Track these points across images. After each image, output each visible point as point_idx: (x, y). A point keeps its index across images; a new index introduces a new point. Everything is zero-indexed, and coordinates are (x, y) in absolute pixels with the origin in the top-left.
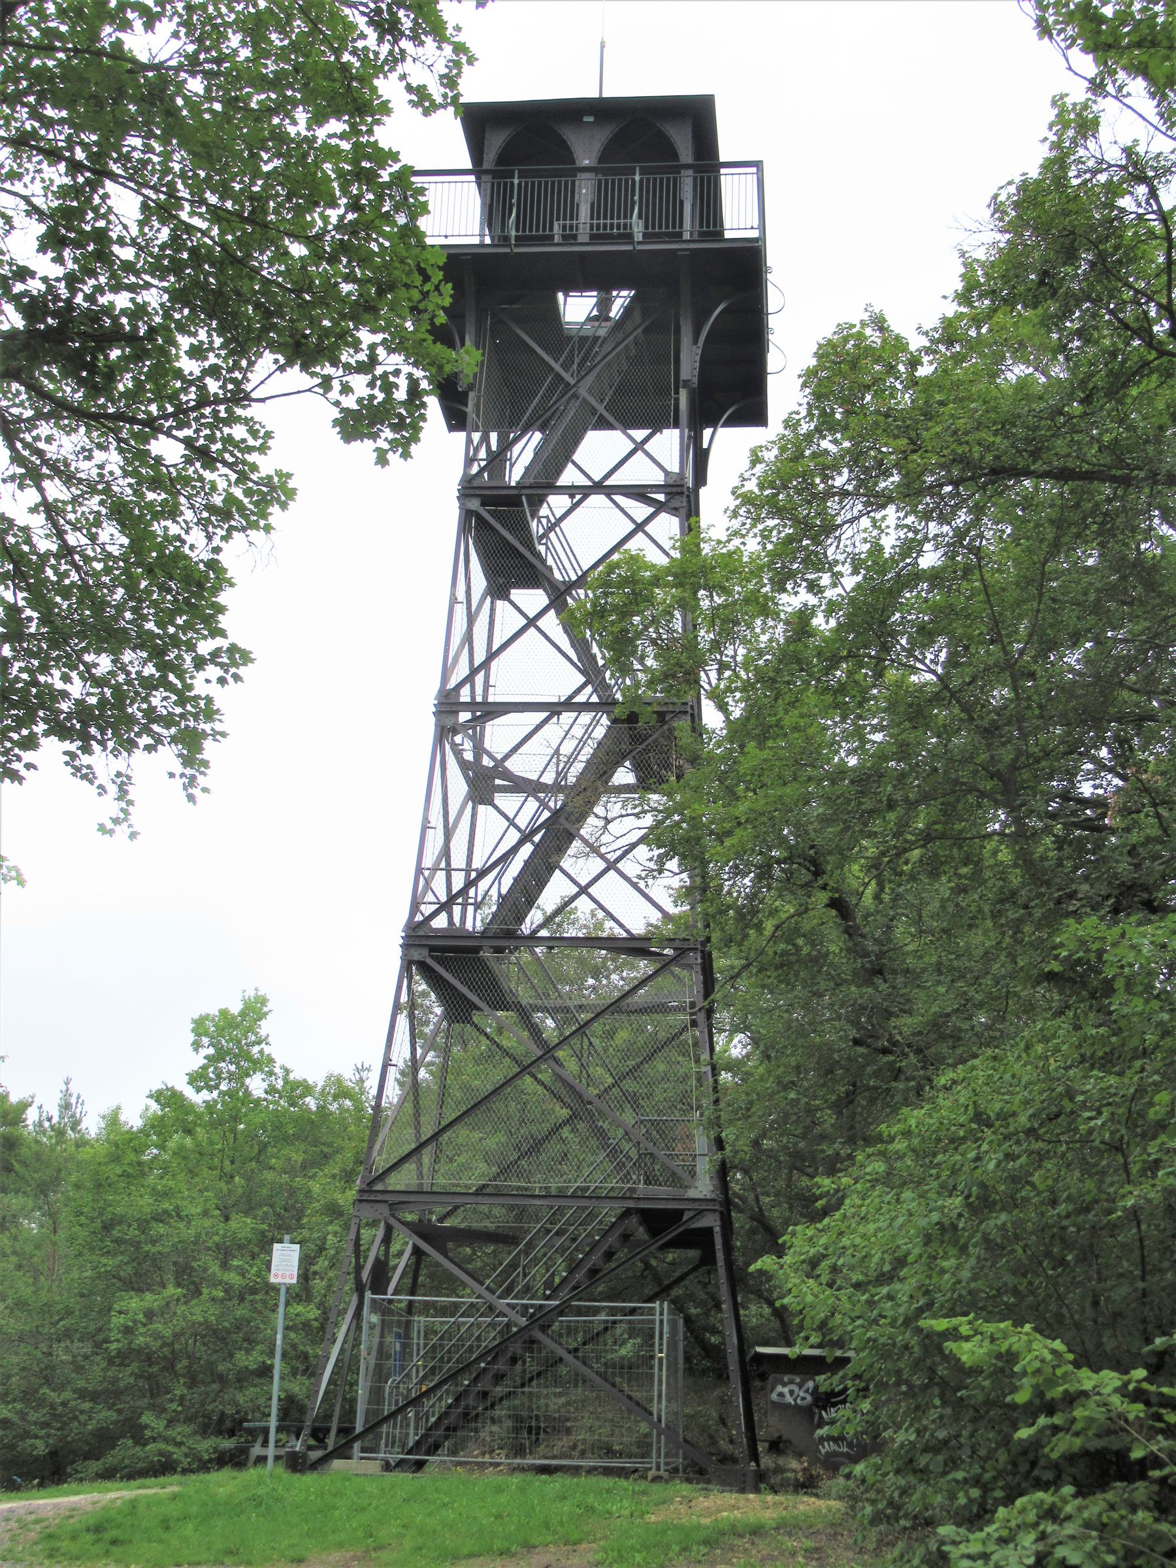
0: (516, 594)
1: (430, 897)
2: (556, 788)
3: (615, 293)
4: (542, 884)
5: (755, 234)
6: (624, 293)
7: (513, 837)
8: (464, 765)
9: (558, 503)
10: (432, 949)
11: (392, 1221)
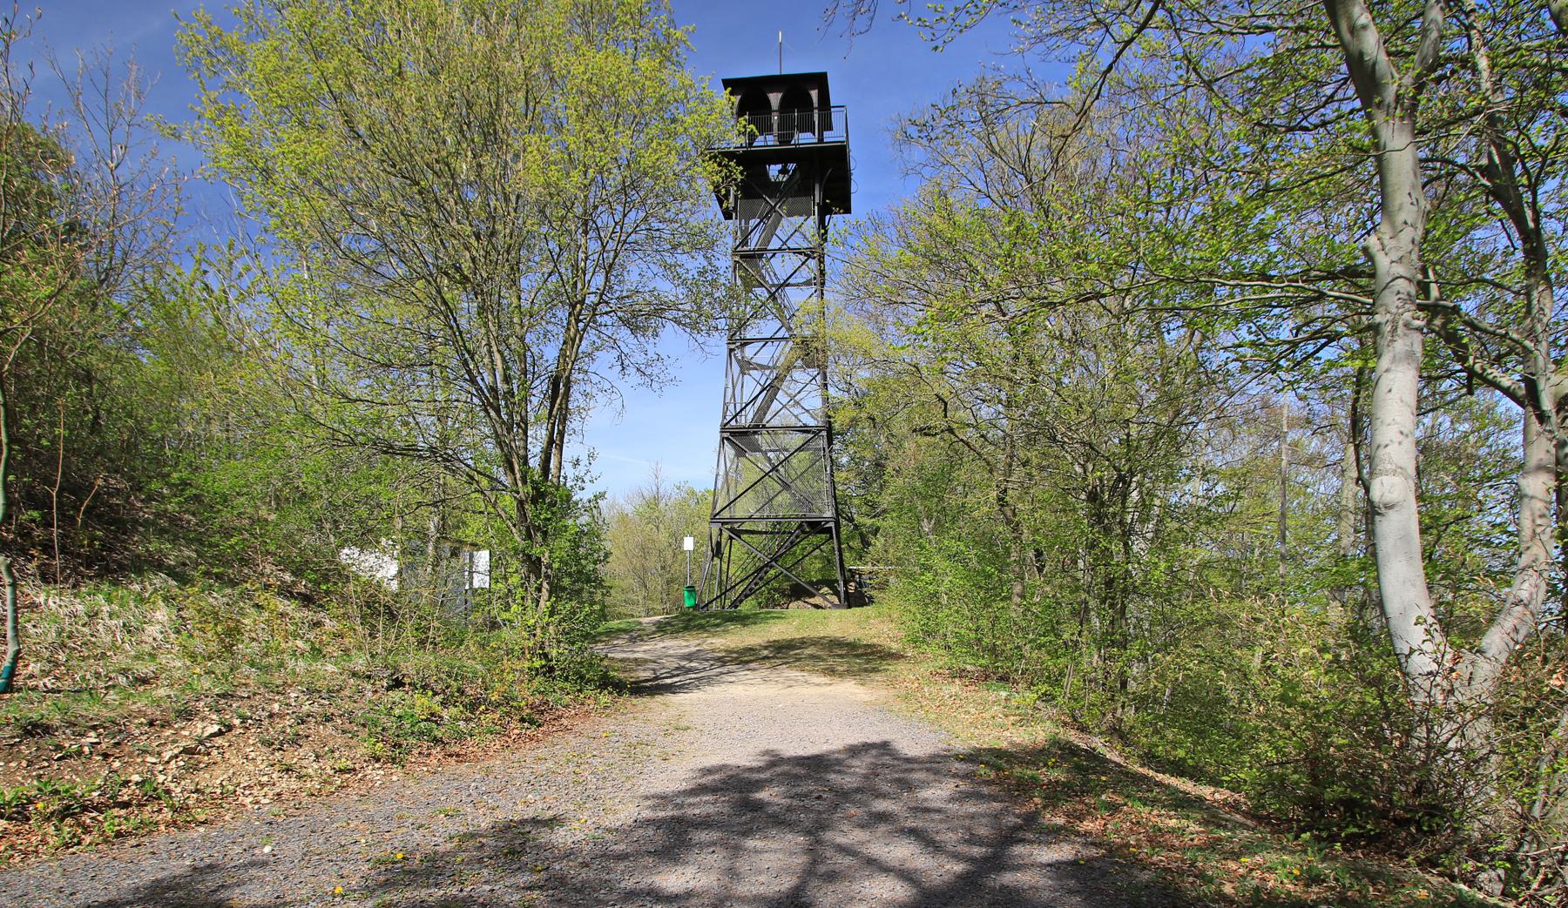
7: (759, 388)
8: (738, 361)
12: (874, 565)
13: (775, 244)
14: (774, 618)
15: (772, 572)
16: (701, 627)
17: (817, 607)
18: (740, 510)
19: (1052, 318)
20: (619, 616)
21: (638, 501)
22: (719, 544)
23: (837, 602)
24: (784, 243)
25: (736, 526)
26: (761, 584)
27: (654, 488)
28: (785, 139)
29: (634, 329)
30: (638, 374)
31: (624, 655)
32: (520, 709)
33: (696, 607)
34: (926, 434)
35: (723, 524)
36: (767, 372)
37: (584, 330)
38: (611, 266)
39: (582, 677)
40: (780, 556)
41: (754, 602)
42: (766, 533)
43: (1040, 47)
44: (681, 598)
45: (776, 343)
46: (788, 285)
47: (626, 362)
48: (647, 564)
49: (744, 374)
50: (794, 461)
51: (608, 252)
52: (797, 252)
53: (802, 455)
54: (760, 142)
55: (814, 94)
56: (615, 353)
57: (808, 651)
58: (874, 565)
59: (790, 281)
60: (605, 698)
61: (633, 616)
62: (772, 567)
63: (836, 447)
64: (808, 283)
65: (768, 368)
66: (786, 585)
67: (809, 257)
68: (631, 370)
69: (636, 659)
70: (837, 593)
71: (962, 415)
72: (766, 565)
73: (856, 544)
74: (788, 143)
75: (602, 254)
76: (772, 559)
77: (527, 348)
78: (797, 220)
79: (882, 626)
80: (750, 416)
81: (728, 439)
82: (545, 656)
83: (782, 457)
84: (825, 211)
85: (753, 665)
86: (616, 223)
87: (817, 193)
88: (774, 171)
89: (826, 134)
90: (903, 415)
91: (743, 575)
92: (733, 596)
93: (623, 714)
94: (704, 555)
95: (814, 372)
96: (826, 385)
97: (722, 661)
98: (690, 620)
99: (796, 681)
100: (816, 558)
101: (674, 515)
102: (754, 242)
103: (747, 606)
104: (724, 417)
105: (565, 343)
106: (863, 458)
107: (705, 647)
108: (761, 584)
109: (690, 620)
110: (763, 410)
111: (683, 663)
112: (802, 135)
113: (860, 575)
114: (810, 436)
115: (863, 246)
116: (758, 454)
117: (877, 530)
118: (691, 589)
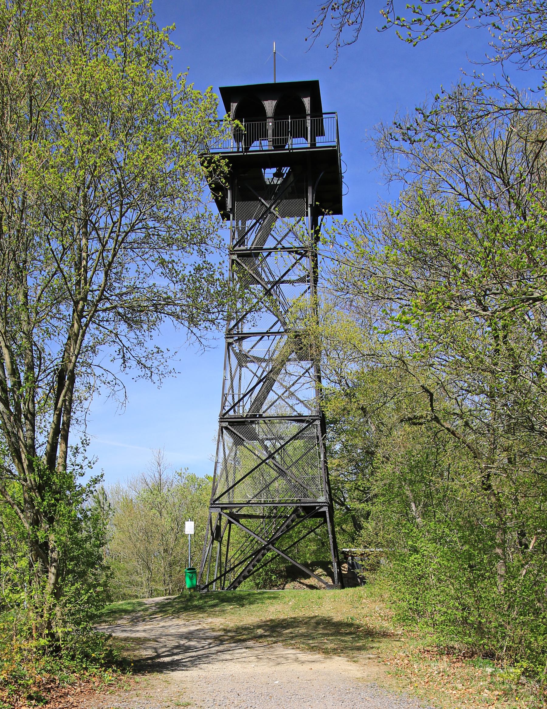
1: (227, 404)
2: (271, 359)
4: (265, 398)
5: (335, 144)
7: (256, 380)
8: (236, 354)
10: (229, 422)
11: (222, 513)
12: (365, 547)
13: (270, 243)
14: (269, 598)
15: (269, 554)
16: (200, 609)
17: (312, 587)
18: (238, 497)
19: (530, 313)
20: (124, 597)
21: (141, 487)
22: (218, 528)
23: (330, 582)
24: (279, 243)
25: (234, 510)
26: (258, 565)
27: (157, 475)
28: (279, 145)
29: (131, 323)
30: (139, 367)
32: (27, 687)
33: (195, 588)
34: (415, 424)
35: (222, 508)
36: (264, 365)
37: (87, 325)
38: (110, 264)
39: (87, 656)
41: (252, 583)
42: (263, 517)
43: (517, 57)
44: (181, 581)
45: (272, 337)
46: (283, 282)
47: (128, 355)
49: (240, 366)
50: (289, 449)
51: (108, 251)
52: (290, 251)
53: (298, 443)
54: (255, 146)
55: (307, 101)
56: (117, 347)
57: (303, 630)
58: (365, 547)
59: (285, 278)
60: (108, 676)
61: (137, 597)
62: (269, 550)
63: (330, 434)
64: (302, 280)
65: (264, 360)
66: (282, 567)
67: (302, 255)
68: (132, 363)
70: (330, 574)
71: (448, 404)
72: (264, 548)
73: (349, 527)
74: (283, 148)
75: (102, 252)
76: (269, 543)
77: (32, 343)
78: (291, 221)
79: (373, 605)
81: (226, 428)
82: (52, 635)
83: (278, 445)
84: (316, 213)
85: (250, 643)
86: (114, 223)
88: (269, 174)
89: (318, 139)
90: (391, 405)
91: (242, 558)
92: (232, 577)
93: (126, 691)
94: (205, 538)
95: (306, 364)
96: (319, 378)
97: (220, 640)
99: (287, 659)
100: (310, 541)
101: (176, 500)
102: (250, 242)
103: (244, 588)
104: (223, 408)
105: (69, 339)
106: (355, 446)
108: (258, 565)
110: (259, 401)
111: (182, 642)
112: (295, 140)
113: (353, 557)
114: (305, 425)
115: (351, 245)
116: (256, 443)
117: (368, 513)
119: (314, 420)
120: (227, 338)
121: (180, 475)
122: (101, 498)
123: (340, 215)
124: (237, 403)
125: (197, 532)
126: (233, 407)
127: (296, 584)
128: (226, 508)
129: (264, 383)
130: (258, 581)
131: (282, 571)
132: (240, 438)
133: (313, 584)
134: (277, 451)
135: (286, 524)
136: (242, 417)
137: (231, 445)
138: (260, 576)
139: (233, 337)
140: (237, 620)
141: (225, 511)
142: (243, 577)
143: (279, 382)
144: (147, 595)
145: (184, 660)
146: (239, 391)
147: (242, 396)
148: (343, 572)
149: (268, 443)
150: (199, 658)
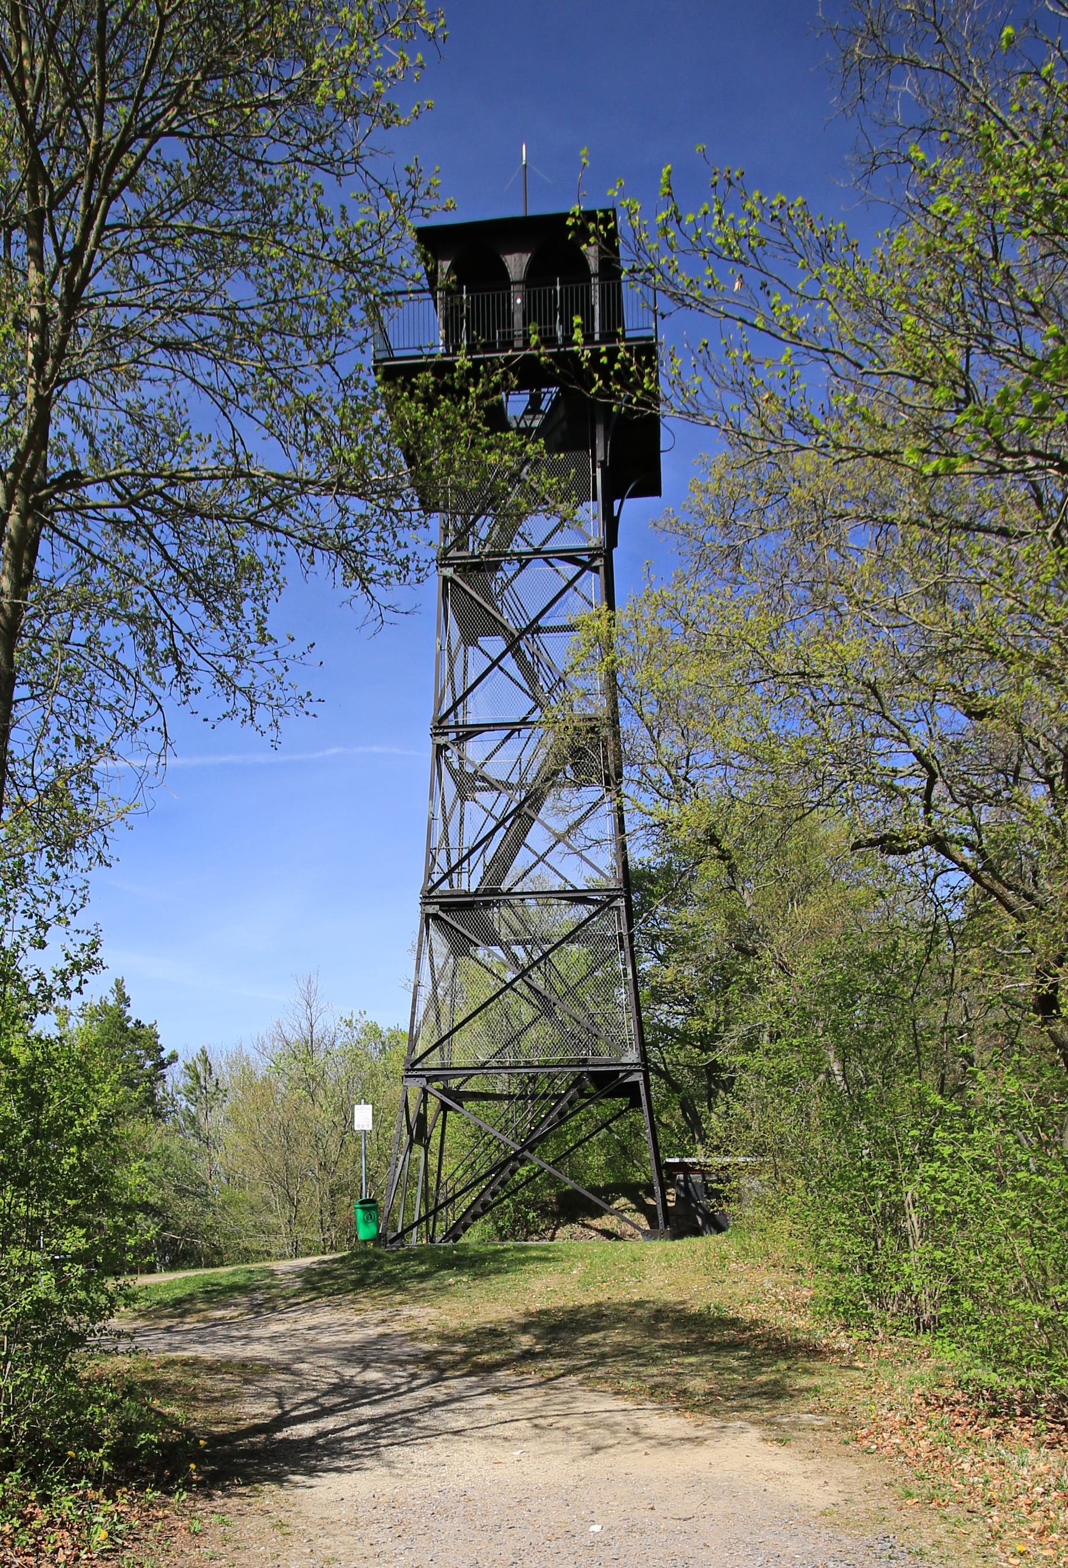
0: (482, 641)
1: (436, 869)
3: (544, 390)
4: (513, 857)
6: (553, 389)
7: (492, 824)
8: (453, 773)
9: (510, 569)
10: (441, 905)
11: (428, 1088)
15: (523, 1171)
16: (391, 1281)
17: (608, 1234)
22: (422, 1119)
27: (305, 1025)
31: (224, 1350)
33: (379, 1239)
40: (542, 1138)
41: (489, 1227)
44: (352, 1223)
48: (293, 1161)
49: (463, 798)
53: (574, 949)
57: (616, 1336)
62: (523, 1162)
65: (508, 786)
66: (549, 1194)
69: (243, 1365)
72: (514, 1158)
79: (756, 1276)
80: (479, 871)
81: (436, 917)
84: (614, 491)
85: (504, 1376)
87: (600, 443)
92: (450, 1216)
98: (368, 1266)
103: (473, 1238)
104: (429, 877)
107: (397, 1327)
109: (368, 1266)
118: (370, 1205)
119: (613, 898)
120: (436, 734)
121: (349, 1024)
122: (200, 1068)
123: (657, 498)
124: (456, 866)
125: (381, 1131)
126: (447, 876)
127: (577, 1228)
128: (436, 1078)
129: (508, 830)
130: (501, 1223)
131: (546, 1204)
132: (464, 936)
133: (608, 1227)
134: (536, 963)
135: (558, 1109)
136: (467, 894)
137: (445, 951)
138: (503, 1213)
139: (447, 734)
140: (464, 1311)
141: (435, 1084)
142: (473, 1215)
143: (542, 823)
144: (288, 1250)
145: (348, 1433)
146: (461, 843)
147: (465, 852)
148: (669, 1204)
149: (518, 950)
150: (381, 1422)
